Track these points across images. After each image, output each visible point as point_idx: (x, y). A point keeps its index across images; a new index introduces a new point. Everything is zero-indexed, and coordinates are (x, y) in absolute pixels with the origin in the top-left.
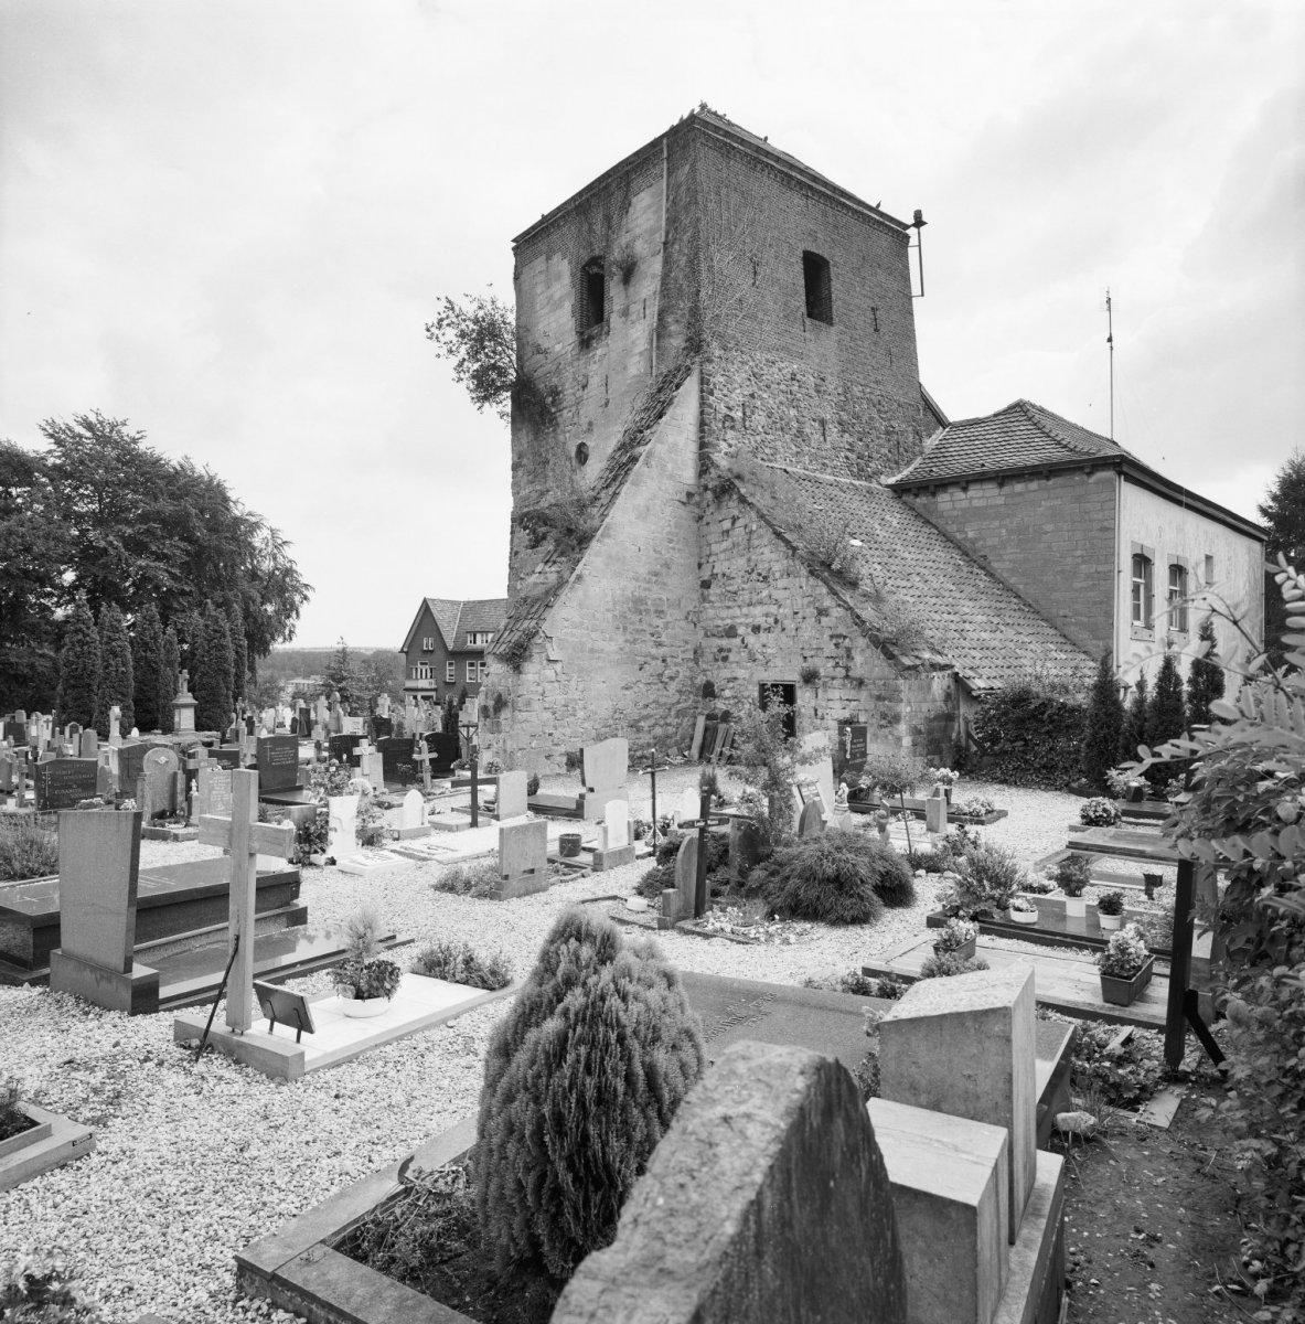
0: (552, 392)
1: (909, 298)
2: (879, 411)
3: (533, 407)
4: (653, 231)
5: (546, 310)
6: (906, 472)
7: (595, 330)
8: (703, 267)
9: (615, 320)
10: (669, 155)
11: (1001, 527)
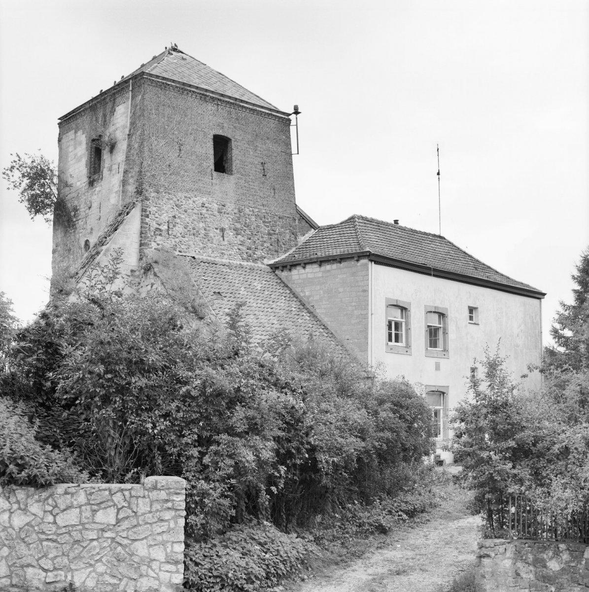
0: (74, 209)
1: (290, 155)
2: (264, 222)
3: (65, 217)
4: (124, 127)
5: (74, 161)
6: (283, 256)
7: (96, 177)
8: (146, 149)
9: (105, 172)
10: (133, 89)
11: (320, 289)
